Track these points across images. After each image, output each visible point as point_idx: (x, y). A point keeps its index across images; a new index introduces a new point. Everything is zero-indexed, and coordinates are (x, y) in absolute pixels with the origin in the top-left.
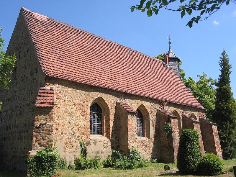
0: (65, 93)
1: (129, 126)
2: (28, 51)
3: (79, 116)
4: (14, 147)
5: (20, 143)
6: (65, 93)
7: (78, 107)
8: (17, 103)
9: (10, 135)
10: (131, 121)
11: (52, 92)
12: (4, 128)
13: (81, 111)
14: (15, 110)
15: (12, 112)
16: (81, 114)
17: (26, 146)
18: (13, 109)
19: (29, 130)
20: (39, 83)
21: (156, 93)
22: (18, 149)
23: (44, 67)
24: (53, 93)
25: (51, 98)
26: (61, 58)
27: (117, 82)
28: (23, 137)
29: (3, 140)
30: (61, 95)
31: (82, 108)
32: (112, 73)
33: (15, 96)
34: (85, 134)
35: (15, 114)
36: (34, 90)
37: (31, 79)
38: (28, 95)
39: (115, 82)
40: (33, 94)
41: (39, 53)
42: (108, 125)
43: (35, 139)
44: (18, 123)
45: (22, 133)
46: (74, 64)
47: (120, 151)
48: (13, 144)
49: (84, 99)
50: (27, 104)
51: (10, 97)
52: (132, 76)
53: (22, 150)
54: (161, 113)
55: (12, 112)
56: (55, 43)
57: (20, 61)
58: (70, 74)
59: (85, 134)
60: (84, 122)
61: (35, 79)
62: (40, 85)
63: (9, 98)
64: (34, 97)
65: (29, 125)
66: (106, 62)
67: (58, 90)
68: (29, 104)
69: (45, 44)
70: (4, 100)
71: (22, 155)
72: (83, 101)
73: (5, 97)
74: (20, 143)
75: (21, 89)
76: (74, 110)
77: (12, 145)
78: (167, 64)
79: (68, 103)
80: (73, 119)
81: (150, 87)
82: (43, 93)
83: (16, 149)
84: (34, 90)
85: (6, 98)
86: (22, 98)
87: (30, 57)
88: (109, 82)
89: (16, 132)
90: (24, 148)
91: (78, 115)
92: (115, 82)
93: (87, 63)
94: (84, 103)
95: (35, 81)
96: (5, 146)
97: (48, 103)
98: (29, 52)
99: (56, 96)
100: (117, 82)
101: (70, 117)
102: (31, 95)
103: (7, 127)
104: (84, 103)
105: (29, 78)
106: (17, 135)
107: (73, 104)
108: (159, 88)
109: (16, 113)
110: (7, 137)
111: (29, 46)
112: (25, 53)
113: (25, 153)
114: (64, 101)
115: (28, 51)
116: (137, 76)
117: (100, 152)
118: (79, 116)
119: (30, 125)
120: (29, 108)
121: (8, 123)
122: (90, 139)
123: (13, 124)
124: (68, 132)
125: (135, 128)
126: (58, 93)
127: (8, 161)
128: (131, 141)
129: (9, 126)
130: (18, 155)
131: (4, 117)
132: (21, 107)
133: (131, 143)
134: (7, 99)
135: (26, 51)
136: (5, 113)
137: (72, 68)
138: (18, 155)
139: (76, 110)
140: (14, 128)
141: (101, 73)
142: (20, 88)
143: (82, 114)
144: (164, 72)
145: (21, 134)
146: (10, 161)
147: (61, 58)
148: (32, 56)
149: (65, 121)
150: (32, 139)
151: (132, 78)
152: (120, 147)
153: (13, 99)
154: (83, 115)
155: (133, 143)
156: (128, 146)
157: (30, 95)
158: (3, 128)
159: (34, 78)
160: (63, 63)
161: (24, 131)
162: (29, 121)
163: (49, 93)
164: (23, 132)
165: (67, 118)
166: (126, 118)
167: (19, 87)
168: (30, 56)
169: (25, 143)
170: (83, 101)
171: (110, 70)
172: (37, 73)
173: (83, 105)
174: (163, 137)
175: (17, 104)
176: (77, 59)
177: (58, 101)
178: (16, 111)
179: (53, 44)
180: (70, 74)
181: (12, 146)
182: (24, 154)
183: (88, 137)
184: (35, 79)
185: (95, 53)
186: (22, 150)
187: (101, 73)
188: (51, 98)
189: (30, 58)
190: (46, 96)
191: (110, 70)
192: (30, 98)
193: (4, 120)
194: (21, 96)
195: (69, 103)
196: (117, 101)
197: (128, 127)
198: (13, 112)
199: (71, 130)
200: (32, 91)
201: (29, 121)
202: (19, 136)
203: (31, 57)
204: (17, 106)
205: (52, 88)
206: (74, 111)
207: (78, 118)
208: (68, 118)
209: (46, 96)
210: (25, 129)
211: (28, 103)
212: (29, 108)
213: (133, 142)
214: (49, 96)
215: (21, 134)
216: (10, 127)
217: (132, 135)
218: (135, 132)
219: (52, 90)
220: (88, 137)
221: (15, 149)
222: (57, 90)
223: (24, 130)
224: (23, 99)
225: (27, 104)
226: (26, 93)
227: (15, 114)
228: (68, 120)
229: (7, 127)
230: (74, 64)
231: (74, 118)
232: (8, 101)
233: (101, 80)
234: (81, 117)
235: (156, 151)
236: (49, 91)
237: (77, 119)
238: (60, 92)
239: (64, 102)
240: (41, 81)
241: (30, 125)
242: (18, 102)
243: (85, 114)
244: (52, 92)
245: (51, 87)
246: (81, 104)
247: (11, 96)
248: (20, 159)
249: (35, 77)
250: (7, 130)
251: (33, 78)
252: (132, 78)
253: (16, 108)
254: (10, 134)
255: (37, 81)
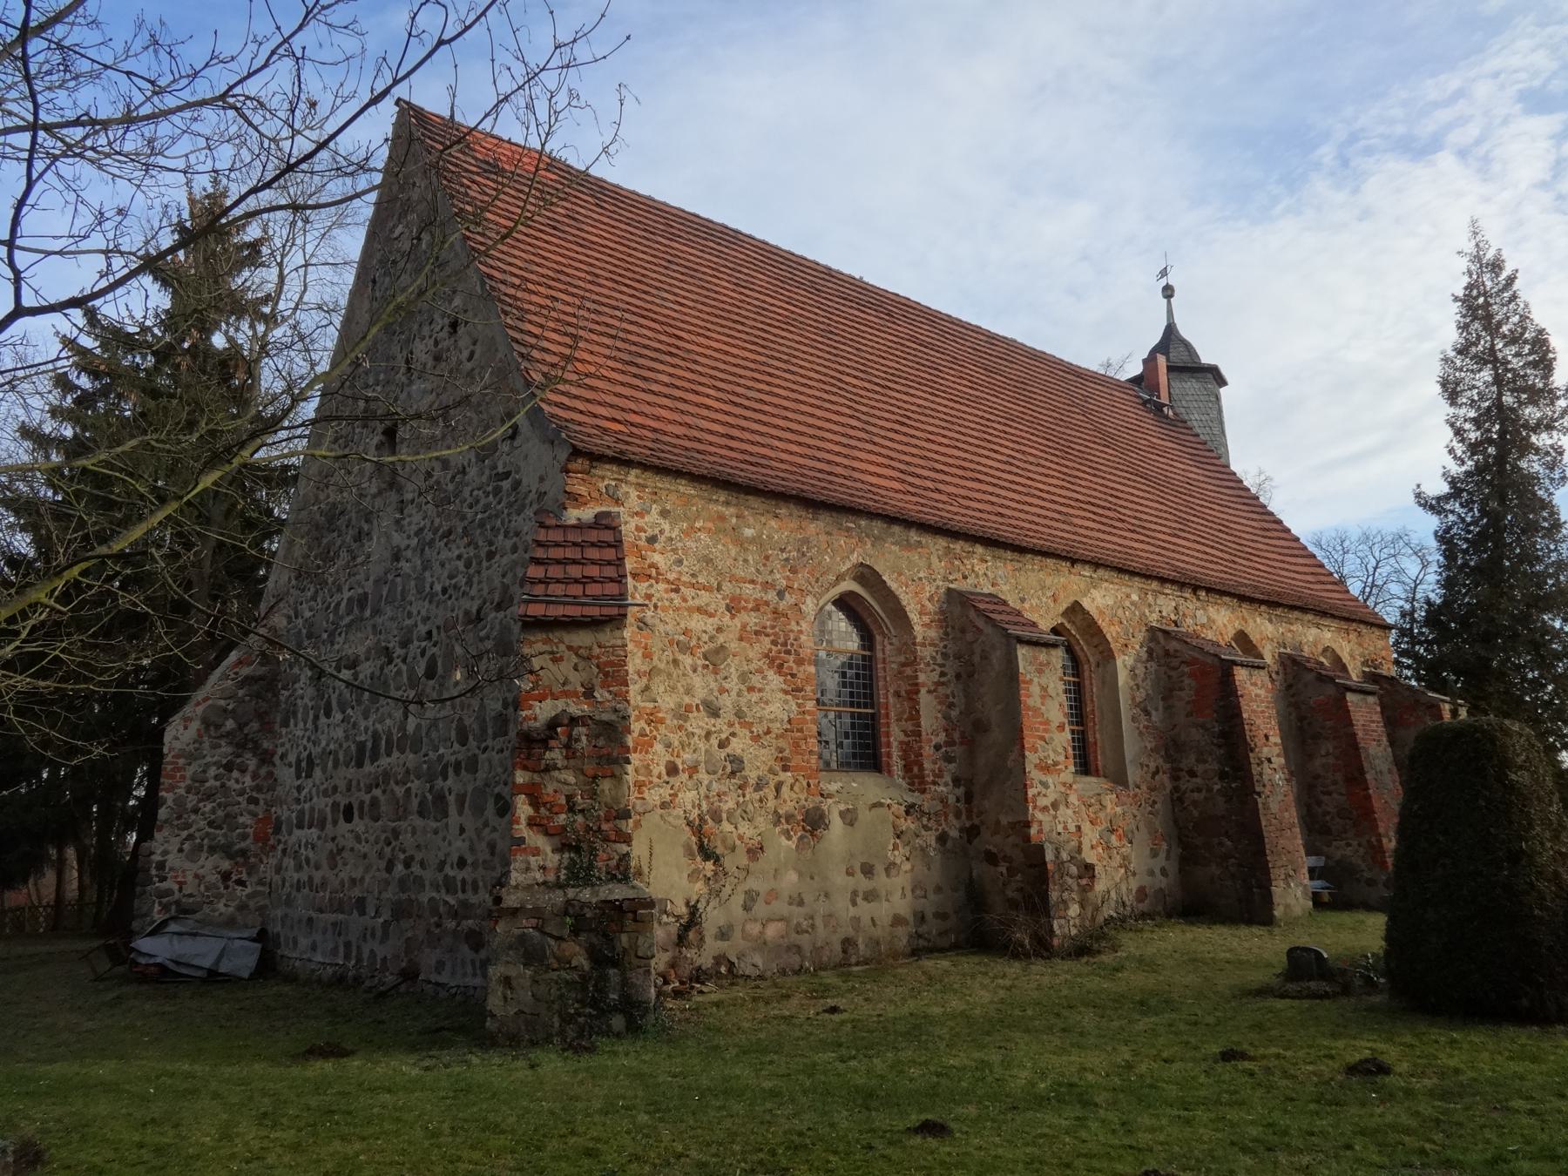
0: (680, 545)
1: (1028, 720)
2: (454, 325)
3: (760, 671)
4: (402, 856)
5: (436, 832)
6: (680, 545)
7: (752, 620)
8: (410, 615)
9: (377, 792)
10: (1035, 689)
11: (608, 536)
12: (341, 757)
13: (767, 640)
14: (399, 651)
15: (382, 669)
16: (767, 656)
17: (472, 849)
18: (387, 648)
19: (482, 757)
20: (533, 496)
21: (1136, 545)
22: (422, 864)
23: (557, 405)
24: (617, 544)
25: (610, 572)
26: (640, 361)
27: (941, 487)
28: (451, 799)
29: (341, 820)
30: (657, 558)
31: (773, 627)
32: (905, 439)
33: (399, 579)
34: (797, 768)
35: (399, 673)
36: (501, 537)
37: (484, 479)
38: (468, 565)
39: (929, 484)
40: (497, 557)
41: (522, 331)
42: (911, 718)
43: (523, 809)
44: (418, 726)
45: (445, 778)
46: (712, 392)
47: (507, 817)
48: (397, 838)
49: (778, 576)
50: (467, 613)
51: (369, 587)
52: (1005, 458)
53: (448, 870)
54: (1173, 645)
55: (382, 669)
56: (600, 285)
57: (414, 387)
58: (699, 441)
59: (797, 768)
60: (786, 702)
61: (507, 475)
62: (535, 507)
63: (360, 591)
64: (504, 576)
65: (484, 730)
66: (867, 385)
67: (639, 529)
68: (479, 611)
69: (550, 287)
70: (338, 604)
71: (446, 903)
72: (773, 586)
73: (339, 590)
74: (436, 832)
75: (429, 536)
76: (730, 640)
77: (389, 844)
78: (1159, 397)
79: (697, 602)
80: (727, 686)
81: (1100, 511)
82: (557, 545)
83: (416, 869)
84: (501, 537)
85: (347, 595)
86: (438, 588)
87: (470, 359)
88: (897, 485)
89: (408, 772)
90: (455, 860)
91: (753, 667)
92: (929, 484)
93: (776, 390)
94: (781, 594)
95: (506, 484)
96: (352, 849)
97: (595, 597)
98: (461, 330)
99: (630, 564)
100: (941, 487)
101: (711, 678)
102: (485, 564)
103: (361, 747)
104: (781, 594)
105: (472, 472)
106: (414, 791)
107: (723, 604)
108: (1145, 517)
109: (404, 668)
110: (362, 803)
111: (457, 301)
112: (436, 343)
113: (464, 891)
114: (677, 591)
115: (454, 325)
116: (1031, 459)
117: (879, 868)
118: (760, 671)
119: (490, 731)
120: (482, 640)
121: (363, 724)
122: (822, 795)
123: (395, 731)
124: (702, 758)
125: (1061, 728)
126: (642, 543)
127: (373, 935)
128: (1042, 802)
129: (369, 745)
130: (424, 898)
131: (340, 695)
132: (435, 632)
133: (1045, 809)
134: (350, 600)
135: (447, 329)
136: (344, 671)
137: (705, 412)
138: (424, 898)
139: (741, 639)
140: (396, 754)
141: (853, 443)
142: (421, 530)
143: (772, 661)
144: (1154, 440)
145: (439, 782)
146: (379, 934)
147: (640, 361)
148: (478, 350)
149: (687, 700)
150: (505, 809)
151: (1008, 468)
152: (979, 834)
153: (385, 593)
154: (781, 666)
155: (1052, 812)
156: (1033, 831)
157: (480, 563)
158: (336, 753)
159: (500, 469)
160: (655, 387)
161: (457, 767)
162: (482, 707)
163: (593, 545)
164: (451, 771)
165: (697, 681)
166: (1011, 677)
167: (414, 528)
168: (466, 354)
169: (462, 830)
170: (773, 586)
171: (897, 427)
172: (516, 444)
173: (775, 612)
174: (1192, 774)
175: (408, 622)
176: (723, 366)
177: (643, 586)
178: (404, 661)
179: (589, 286)
180: (699, 441)
181: (388, 850)
182: (460, 895)
183: (809, 785)
184: (507, 475)
185: (807, 341)
186: (448, 870)
187: (853, 443)
188: (610, 572)
189: (469, 366)
190: (575, 562)
191: (897, 427)
192: (480, 582)
193: (343, 712)
194: (427, 574)
195: (704, 598)
196: (951, 586)
197: (1025, 720)
198: (390, 662)
199: (722, 745)
200: (491, 544)
201: (482, 707)
202: (430, 797)
203: (476, 356)
204: (410, 630)
205: (608, 514)
206: (734, 646)
207: (756, 680)
208: (702, 686)
209: (575, 562)
210: (460, 757)
211: (474, 610)
212: (482, 640)
213: (1055, 805)
214: (594, 562)
215: (439, 782)
216: (376, 746)
217: (1046, 768)
218: (1060, 750)
219: (607, 527)
220: (809, 785)
221: (407, 865)
222: (632, 526)
223: (453, 759)
224: (444, 591)
225: (467, 613)
226: (459, 557)
227: (399, 673)
228: (700, 694)
229: (361, 747)
230: (712, 392)
231: (733, 684)
232: (362, 607)
233: (856, 475)
234: (771, 674)
235: (1162, 855)
236: (593, 536)
237: (751, 689)
238: (652, 540)
239: (673, 595)
240: (542, 479)
241: (490, 731)
242: (415, 613)
243: (792, 658)
244: (608, 536)
245: (598, 509)
246: (767, 603)
247: (372, 579)
248: (438, 925)
249: (505, 465)
250: (360, 765)
251: (495, 467)
252: (1008, 468)
253: (405, 644)
254: (377, 786)
255: (517, 485)
